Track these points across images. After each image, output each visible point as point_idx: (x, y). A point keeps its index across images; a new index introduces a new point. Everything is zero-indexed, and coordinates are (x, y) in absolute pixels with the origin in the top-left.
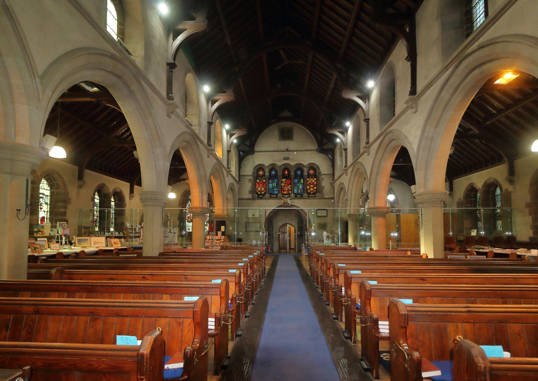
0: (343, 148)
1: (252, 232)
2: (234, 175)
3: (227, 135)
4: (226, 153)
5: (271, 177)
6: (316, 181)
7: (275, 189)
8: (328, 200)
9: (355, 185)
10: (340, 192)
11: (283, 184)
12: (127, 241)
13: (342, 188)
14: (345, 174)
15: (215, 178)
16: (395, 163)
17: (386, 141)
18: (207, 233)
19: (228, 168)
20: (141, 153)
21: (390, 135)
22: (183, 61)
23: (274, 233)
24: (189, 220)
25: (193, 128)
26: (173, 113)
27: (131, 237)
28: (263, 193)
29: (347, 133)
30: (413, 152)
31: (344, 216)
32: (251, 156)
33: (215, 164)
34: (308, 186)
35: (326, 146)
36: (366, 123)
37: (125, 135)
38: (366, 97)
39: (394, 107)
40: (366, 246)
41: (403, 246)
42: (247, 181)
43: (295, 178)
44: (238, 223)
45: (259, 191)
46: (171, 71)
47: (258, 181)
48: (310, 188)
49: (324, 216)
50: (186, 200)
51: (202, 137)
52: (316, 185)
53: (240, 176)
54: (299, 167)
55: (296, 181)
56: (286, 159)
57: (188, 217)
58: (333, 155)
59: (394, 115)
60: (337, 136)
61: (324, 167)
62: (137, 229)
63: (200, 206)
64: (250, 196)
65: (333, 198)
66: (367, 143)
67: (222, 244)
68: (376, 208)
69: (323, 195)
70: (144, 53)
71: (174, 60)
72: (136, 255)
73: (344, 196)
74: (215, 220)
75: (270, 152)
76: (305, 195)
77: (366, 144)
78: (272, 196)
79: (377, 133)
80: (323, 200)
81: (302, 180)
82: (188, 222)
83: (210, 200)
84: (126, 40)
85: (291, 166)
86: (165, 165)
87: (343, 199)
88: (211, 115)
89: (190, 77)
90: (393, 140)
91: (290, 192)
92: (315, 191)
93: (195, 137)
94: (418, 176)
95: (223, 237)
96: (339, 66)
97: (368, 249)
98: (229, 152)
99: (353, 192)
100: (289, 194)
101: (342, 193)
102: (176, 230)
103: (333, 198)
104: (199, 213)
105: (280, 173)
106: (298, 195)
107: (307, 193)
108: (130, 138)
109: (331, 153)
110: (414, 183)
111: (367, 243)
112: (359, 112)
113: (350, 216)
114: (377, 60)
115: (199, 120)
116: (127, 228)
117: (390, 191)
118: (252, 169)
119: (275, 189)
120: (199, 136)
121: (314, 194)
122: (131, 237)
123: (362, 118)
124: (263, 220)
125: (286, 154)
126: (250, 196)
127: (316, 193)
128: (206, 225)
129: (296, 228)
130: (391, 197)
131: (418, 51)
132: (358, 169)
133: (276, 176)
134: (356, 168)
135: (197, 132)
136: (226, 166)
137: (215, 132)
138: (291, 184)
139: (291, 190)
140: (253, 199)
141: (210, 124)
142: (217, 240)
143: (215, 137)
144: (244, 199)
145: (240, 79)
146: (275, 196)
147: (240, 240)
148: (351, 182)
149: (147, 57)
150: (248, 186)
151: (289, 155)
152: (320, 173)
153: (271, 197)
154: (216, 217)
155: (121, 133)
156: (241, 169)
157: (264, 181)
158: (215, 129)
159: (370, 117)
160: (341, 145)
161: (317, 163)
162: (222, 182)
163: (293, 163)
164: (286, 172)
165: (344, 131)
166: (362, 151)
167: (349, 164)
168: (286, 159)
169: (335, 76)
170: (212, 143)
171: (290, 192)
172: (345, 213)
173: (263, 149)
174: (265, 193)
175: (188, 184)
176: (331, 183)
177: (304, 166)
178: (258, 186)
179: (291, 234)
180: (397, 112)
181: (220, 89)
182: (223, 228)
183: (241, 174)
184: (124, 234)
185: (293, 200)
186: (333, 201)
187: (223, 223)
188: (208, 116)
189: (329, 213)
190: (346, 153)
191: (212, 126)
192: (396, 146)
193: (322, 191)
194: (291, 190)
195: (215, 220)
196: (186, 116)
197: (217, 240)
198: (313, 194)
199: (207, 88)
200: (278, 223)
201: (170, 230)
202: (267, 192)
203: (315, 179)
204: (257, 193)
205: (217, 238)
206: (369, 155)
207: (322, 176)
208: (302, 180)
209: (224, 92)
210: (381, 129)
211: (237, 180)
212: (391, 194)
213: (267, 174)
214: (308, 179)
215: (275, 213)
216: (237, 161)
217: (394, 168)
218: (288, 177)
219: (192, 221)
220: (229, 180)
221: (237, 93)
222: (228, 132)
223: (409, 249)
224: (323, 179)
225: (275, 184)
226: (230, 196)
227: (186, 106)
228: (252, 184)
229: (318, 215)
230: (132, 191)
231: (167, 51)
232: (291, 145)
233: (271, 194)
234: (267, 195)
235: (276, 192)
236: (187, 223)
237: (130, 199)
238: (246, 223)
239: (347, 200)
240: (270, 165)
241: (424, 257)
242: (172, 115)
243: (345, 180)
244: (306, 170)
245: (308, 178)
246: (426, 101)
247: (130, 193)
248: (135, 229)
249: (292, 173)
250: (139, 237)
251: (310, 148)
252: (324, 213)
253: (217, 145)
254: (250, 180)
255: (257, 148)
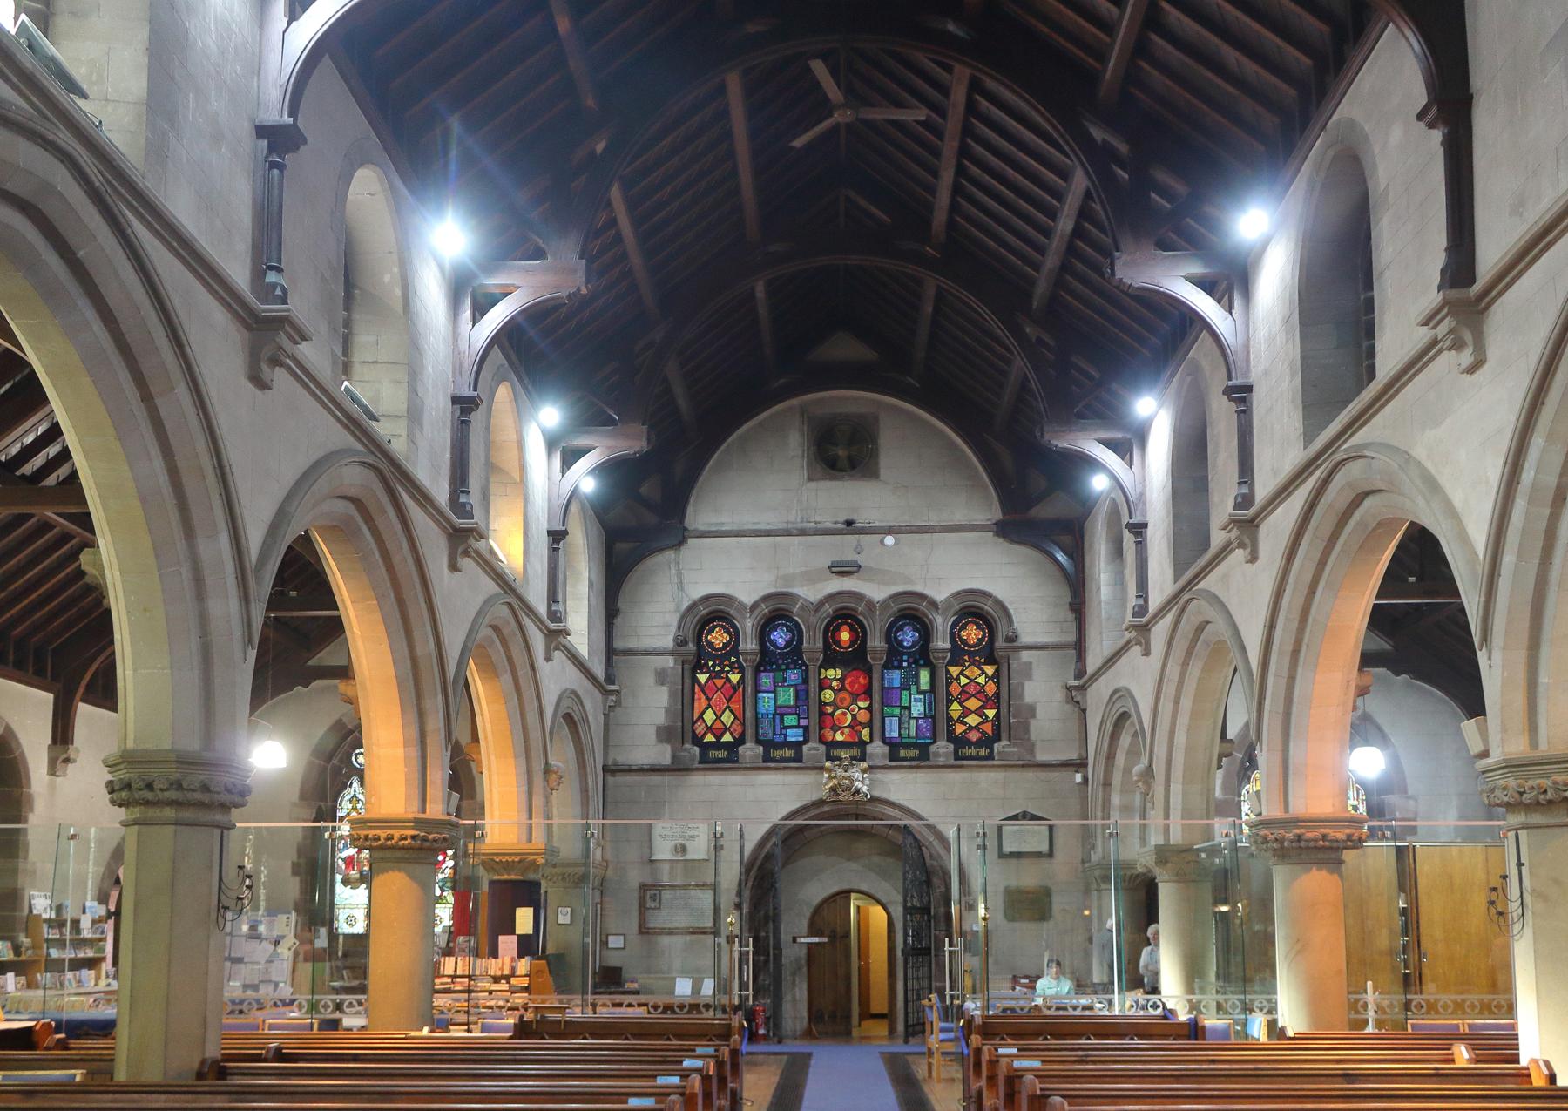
0: (1125, 520)
1: (671, 932)
2: (583, 649)
3: (547, 465)
4: (541, 542)
5: (767, 659)
6: (996, 677)
7: (790, 720)
8: (1054, 775)
9: (1186, 703)
10: (1114, 737)
11: (828, 696)
12: (31, 985)
13: (1124, 717)
14: (1136, 650)
15: (489, 669)
16: (1378, 598)
17: (1336, 494)
18: (442, 941)
19: (555, 616)
20: (114, 561)
21: (1354, 470)
22: (339, 115)
23: (785, 938)
24: (354, 874)
25: (382, 429)
26: (282, 364)
27: (55, 966)
28: (727, 737)
29: (1135, 459)
30: (1466, 538)
31: (1140, 855)
32: (670, 554)
33: (488, 602)
34: (955, 706)
35: (1038, 507)
36: (1233, 406)
37: (38, 461)
38: (1230, 281)
39: (1370, 332)
40: (1247, 1009)
41: (1432, 1008)
42: (651, 679)
43: (888, 666)
44: (602, 886)
45: (709, 729)
46: (273, 165)
47: (703, 678)
48: (966, 712)
49: (1039, 855)
50: (337, 772)
51: (422, 475)
52: (995, 701)
53: (611, 653)
54: (911, 612)
55: (895, 677)
56: (844, 569)
57: (349, 861)
58: (1077, 552)
59: (1372, 374)
60: (1092, 464)
61: (1031, 609)
62: (86, 923)
63: (413, 812)
64: (662, 754)
65: (1081, 765)
66: (1245, 501)
67: (519, 999)
68: (1296, 822)
69: (1032, 750)
70: (145, 84)
71: (293, 112)
72: (78, 1075)
73: (1134, 753)
74: (485, 878)
75: (758, 539)
76: (943, 748)
77: (1237, 506)
78: (775, 754)
79: (1295, 456)
80: (1030, 774)
81: (924, 676)
82: (346, 882)
83: (463, 780)
84: (62, 22)
85: (871, 605)
86: (235, 619)
87: (1127, 771)
88: (469, 363)
89: (368, 188)
90: (1367, 494)
91: (865, 733)
92: (988, 728)
93: (392, 474)
94: (1496, 671)
95: (523, 965)
96: (1098, 134)
97: (1258, 1028)
98: (557, 537)
99: (1181, 738)
100: (862, 744)
101: (1125, 740)
102: (286, 925)
103: (1081, 765)
104: (405, 850)
105: (813, 642)
106: (908, 746)
107: (951, 737)
108: (63, 472)
109: (1067, 539)
110: (1474, 705)
111: (1258, 1000)
112: (1200, 350)
113: (1164, 854)
114: (1285, 108)
115: (413, 391)
116: (32, 921)
117: (1363, 729)
118: (674, 620)
119: (790, 720)
120: (409, 467)
121: (987, 742)
122: (55, 966)
123: (1216, 384)
124: (730, 874)
125: (845, 548)
126: (662, 754)
127: (997, 737)
128: (439, 900)
129: (898, 912)
130: (1368, 763)
131: (1478, 80)
132: (1201, 628)
133: (794, 653)
134: (1186, 627)
135: (398, 447)
136: (542, 610)
137: (488, 445)
138: (868, 693)
139: (870, 724)
140: (678, 768)
141: (465, 406)
142: (496, 980)
143: (491, 468)
144: (629, 770)
145: (615, 193)
146: (789, 753)
147: (610, 979)
148: (1169, 689)
149: (162, 101)
150: (652, 704)
151: (858, 549)
152: (1012, 639)
153: (767, 758)
154: (490, 865)
155: (15, 449)
156: (618, 621)
157: (735, 678)
158: (488, 428)
159: (1253, 378)
160: (1114, 501)
161: (999, 590)
162: (523, 687)
163: (877, 592)
164: (845, 636)
165: (1129, 443)
166: (1218, 538)
167: (1155, 600)
168: (844, 569)
169: (1080, 182)
170: (474, 498)
171: (865, 733)
172: (1143, 840)
173: (727, 521)
174: (740, 741)
175: (352, 701)
176: (1069, 689)
177: (933, 604)
178: (701, 702)
179: (874, 993)
180: (1388, 361)
181: (514, 243)
182: (524, 919)
183: (619, 644)
184: (17, 949)
185: (880, 775)
186: (1078, 778)
187: (528, 893)
188: (457, 369)
189: (1059, 841)
190: (1141, 545)
191: (476, 418)
192: (1384, 526)
193: (1027, 730)
194: (870, 724)
195: (485, 878)
196: (347, 369)
197: (496, 980)
198: (979, 744)
199: (447, 237)
200: (809, 888)
201: (253, 928)
202: (750, 732)
203: (990, 670)
204: (697, 740)
205: (494, 966)
206: (1253, 558)
207: (1025, 656)
208: (924, 676)
209: (538, 254)
210: (1308, 438)
211: (599, 670)
212: (1367, 743)
213: (749, 644)
214: (955, 671)
215: (790, 844)
216: (600, 584)
217: (1380, 619)
218: (855, 659)
219: (366, 879)
220: (556, 678)
221: (601, 253)
222: (551, 443)
223: (1463, 1025)
224: (1027, 670)
225: (787, 696)
226: (562, 756)
227: (347, 324)
228: (672, 695)
229: (1007, 849)
230: (62, 733)
231: (256, 67)
232: (867, 499)
233: (768, 745)
234: (750, 751)
235: (794, 735)
236: (339, 887)
237: (52, 771)
238: (644, 888)
239: (1149, 772)
240: (766, 598)
241: (1538, 1081)
242: (280, 377)
243: (1138, 676)
244: (941, 624)
245: (952, 663)
246: (1522, 324)
247: (54, 740)
248: (76, 923)
249: (876, 643)
250: (92, 963)
251: (959, 517)
252: (1031, 838)
253: (496, 505)
254: (661, 677)
255: (699, 516)
